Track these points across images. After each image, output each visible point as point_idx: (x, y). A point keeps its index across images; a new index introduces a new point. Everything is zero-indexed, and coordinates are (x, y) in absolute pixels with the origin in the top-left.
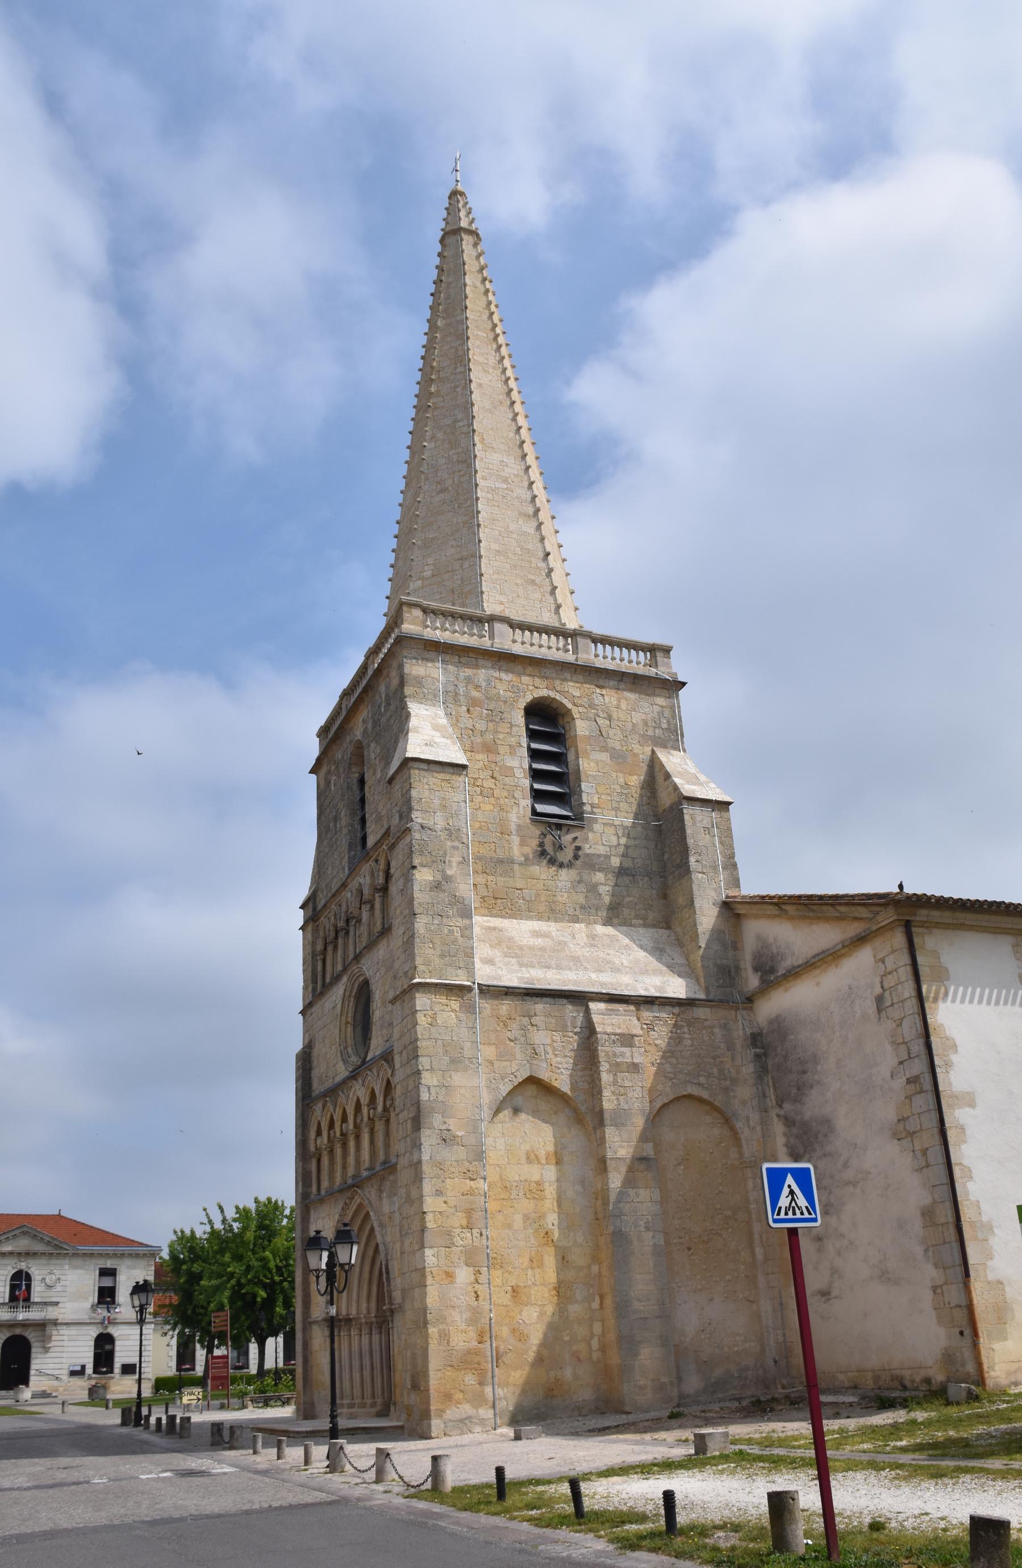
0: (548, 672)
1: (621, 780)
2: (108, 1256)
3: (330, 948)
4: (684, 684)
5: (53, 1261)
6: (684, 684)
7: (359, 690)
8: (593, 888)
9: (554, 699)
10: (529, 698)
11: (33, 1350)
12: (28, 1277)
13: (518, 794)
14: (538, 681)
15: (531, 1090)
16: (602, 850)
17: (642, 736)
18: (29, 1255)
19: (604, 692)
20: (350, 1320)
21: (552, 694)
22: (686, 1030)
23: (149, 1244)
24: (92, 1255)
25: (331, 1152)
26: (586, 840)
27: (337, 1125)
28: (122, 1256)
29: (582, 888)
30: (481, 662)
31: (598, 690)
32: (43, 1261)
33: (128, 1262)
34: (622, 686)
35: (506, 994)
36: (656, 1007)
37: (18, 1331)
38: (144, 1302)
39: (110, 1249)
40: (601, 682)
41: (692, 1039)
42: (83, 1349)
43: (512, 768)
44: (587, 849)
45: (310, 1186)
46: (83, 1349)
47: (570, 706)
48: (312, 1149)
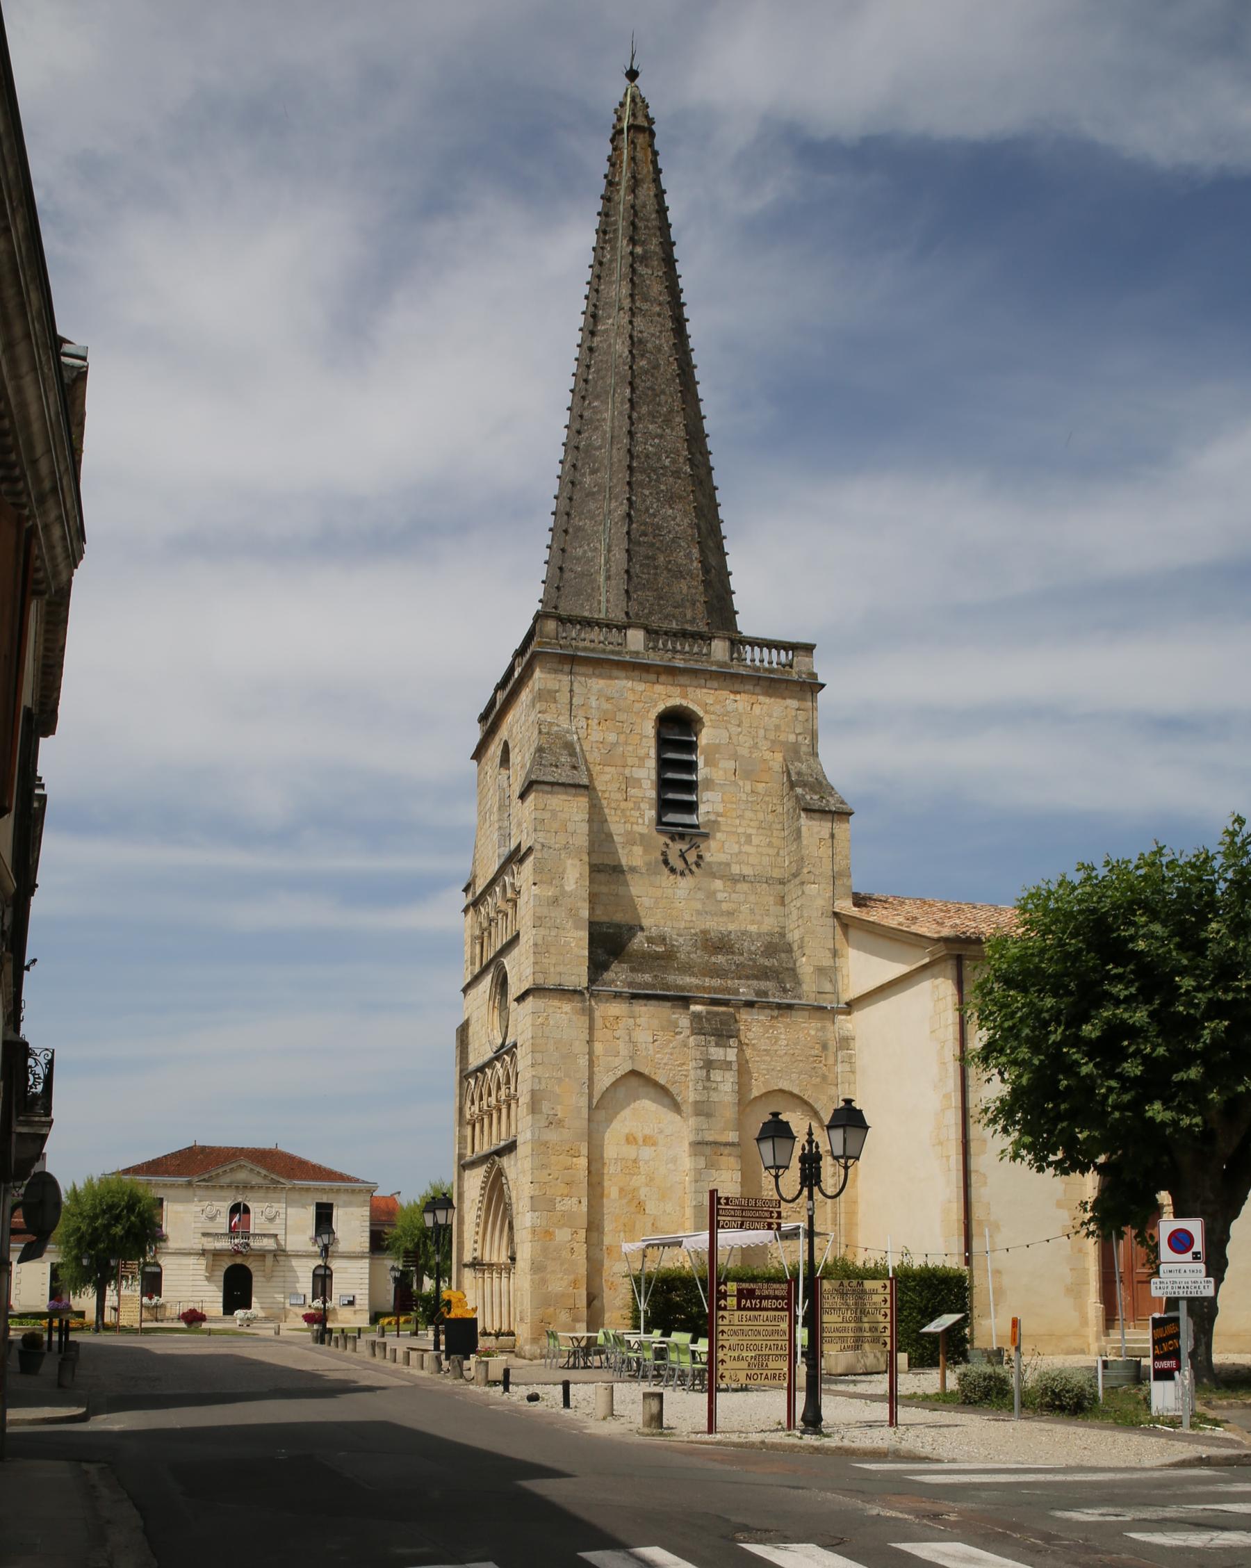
0: (683, 680)
1: (748, 788)
2: (323, 1190)
3: (486, 934)
4: (823, 686)
5: (271, 1195)
6: (823, 686)
7: (492, 716)
8: (711, 895)
9: (687, 708)
10: (661, 707)
11: (254, 1279)
12: (247, 1210)
13: (644, 806)
14: (671, 690)
15: (634, 1082)
16: (722, 857)
17: (773, 742)
18: (246, 1187)
19: (738, 697)
20: (492, 1265)
21: (684, 703)
22: (783, 1030)
23: (361, 1178)
24: (308, 1190)
25: (500, 1110)
26: (708, 849)
27: (485, 1097)
28: (338, 1191)
29: (700, 895)
30: (615, 673)
31: (732, 696)
32: (261, 1194)
33: (344, 1197)
34: (758, 690)
35: (615, 997)
36: (755, 1011)
37: (239, 1260)
38: (326, 1242)
39: (326, 1184)
40: (737, 687)
41: (788, 1040)
42: (496, 1288)
43: (639, 780)
44: (708, 857)
45: (466, 1148)
46: (496, 1288)
47: (701, 714)
48: (468, 1117)
